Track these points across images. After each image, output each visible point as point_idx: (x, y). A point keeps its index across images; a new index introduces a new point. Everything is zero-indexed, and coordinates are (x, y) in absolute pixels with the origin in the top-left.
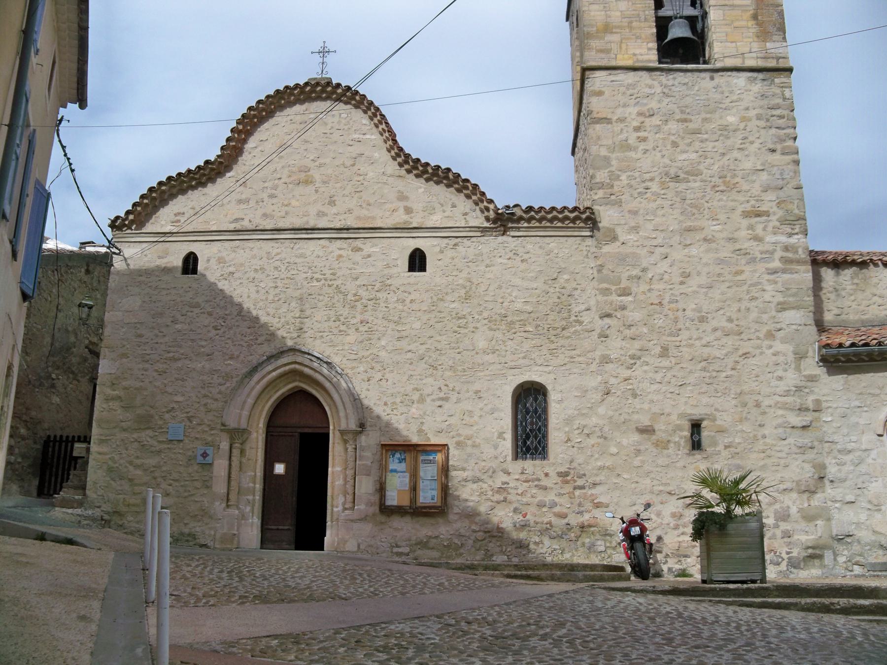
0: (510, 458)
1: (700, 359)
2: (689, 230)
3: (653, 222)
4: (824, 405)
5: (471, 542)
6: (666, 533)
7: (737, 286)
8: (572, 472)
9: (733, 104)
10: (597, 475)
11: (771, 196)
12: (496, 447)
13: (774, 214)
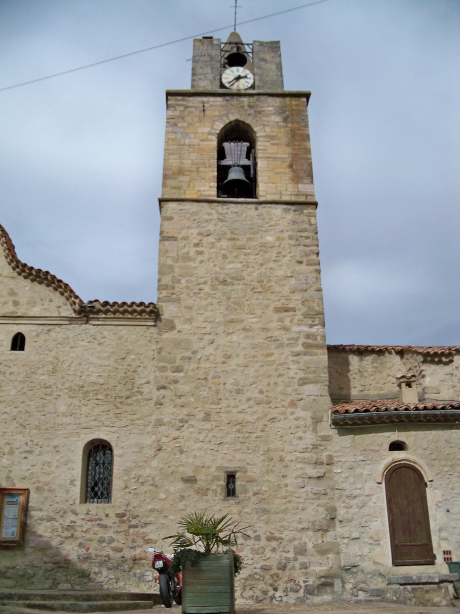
0: (78, 501)
1: (235, 423)
2: (232, 321)
3: (204, 315)
4: (336, 459)
5: (41, 572)
7: (268, 365)
8: (128, 513)
9: (272, 228)
10: (148, 516)
11: (298, 296)
12: (67, 492)
13: (300, 310)
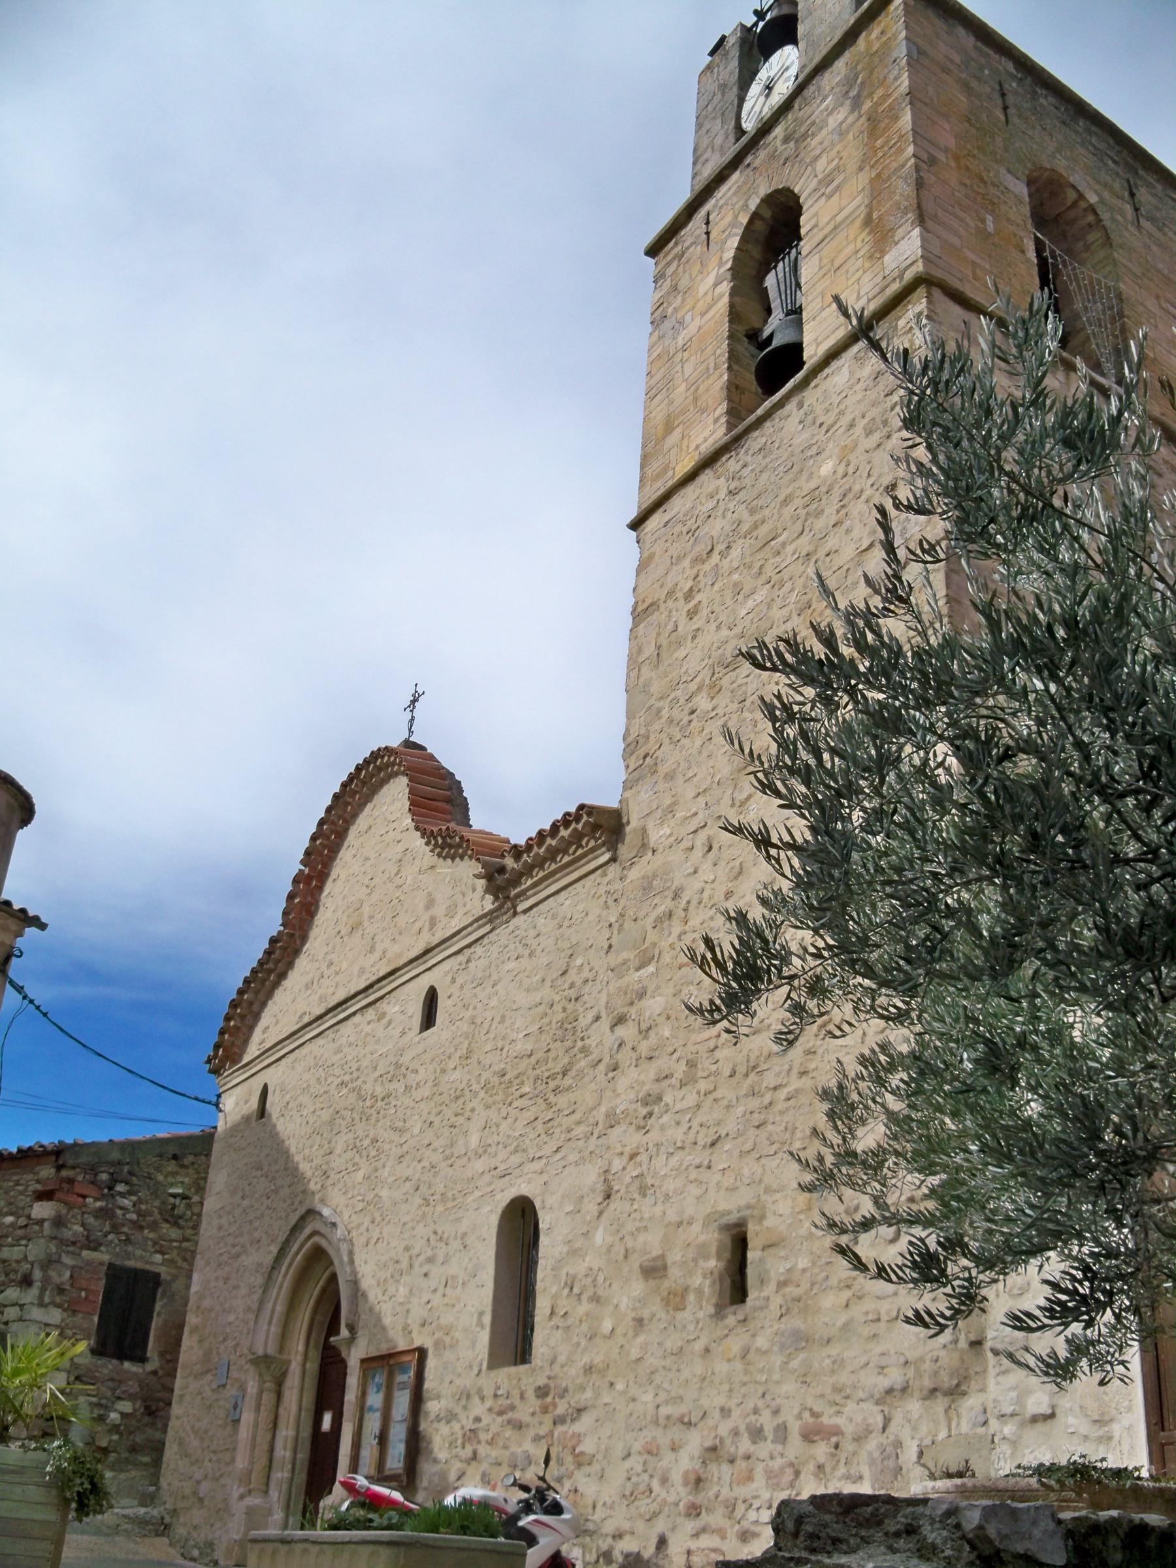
6: (673, 1529)
